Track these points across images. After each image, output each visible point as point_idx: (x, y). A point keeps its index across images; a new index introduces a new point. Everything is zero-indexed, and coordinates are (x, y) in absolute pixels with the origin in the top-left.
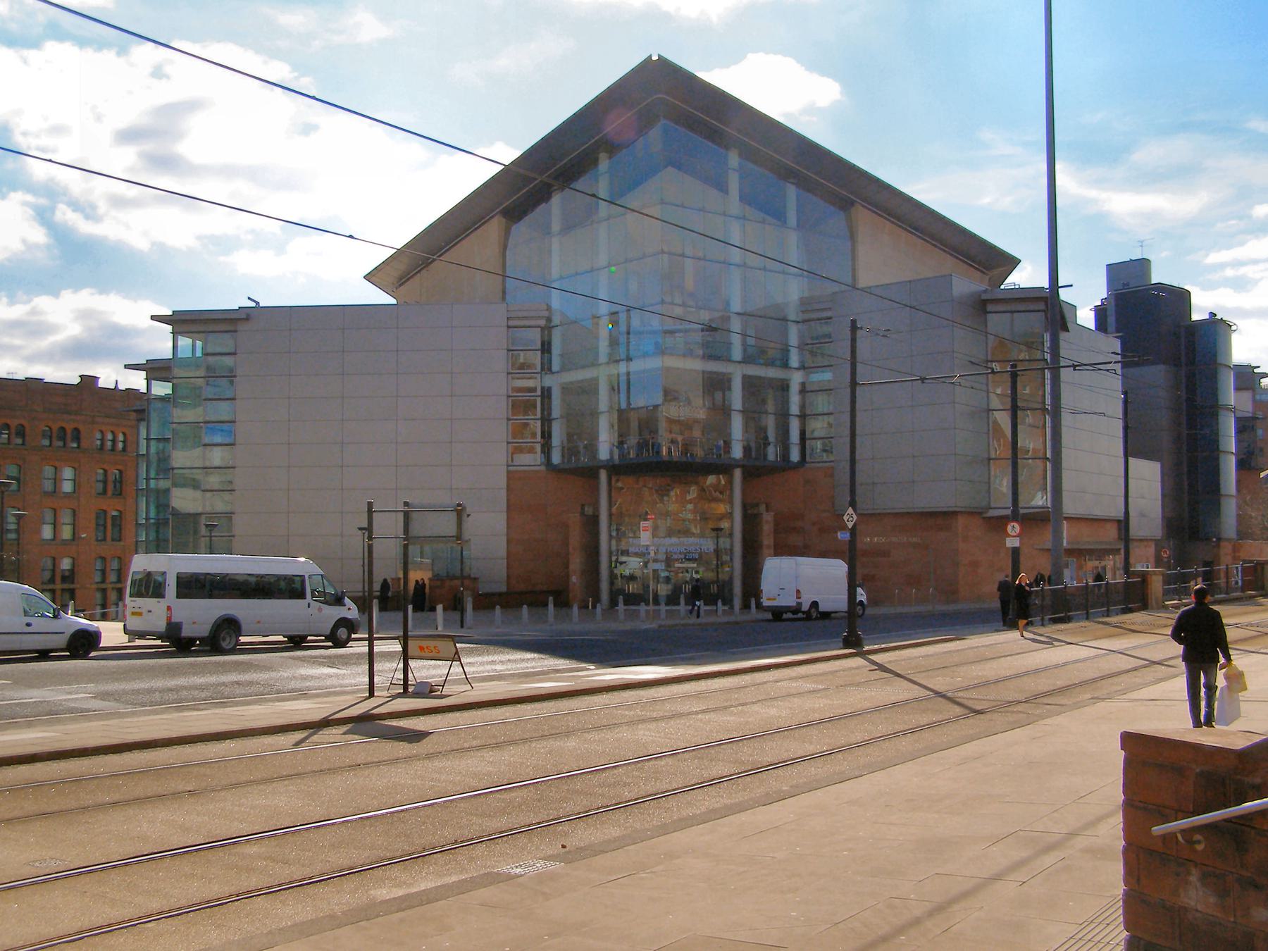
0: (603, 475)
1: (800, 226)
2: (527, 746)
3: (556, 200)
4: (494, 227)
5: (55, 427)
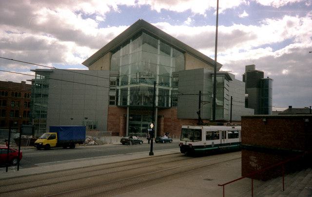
0: (157, 109)
1: (173, 56)
2: (51, 166)
3: (121, 49)
4: (108, 55)
5: (15, 92)
